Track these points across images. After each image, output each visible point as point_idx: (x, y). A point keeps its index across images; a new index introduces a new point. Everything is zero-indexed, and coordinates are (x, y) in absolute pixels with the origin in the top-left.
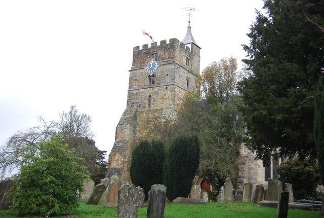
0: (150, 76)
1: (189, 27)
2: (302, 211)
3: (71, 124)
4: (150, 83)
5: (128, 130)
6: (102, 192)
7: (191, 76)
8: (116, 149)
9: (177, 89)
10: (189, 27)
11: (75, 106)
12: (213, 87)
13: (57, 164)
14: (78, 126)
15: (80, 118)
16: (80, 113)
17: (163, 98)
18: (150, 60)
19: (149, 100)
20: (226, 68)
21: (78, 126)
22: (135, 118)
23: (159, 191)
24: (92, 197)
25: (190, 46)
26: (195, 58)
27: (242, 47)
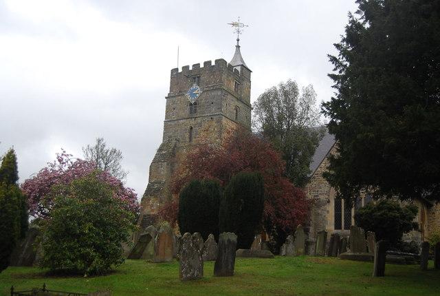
0: (191, 104)
1: (238, 47)
2: (356, 263)
3: (97, 160)
4: (191, 113)
5: (164, 170)
6: (147, 243)
7: (240, 105)
8: (150, 191)
9: (224, 121)
10: (238, 47)
11: (102, 139)
12: (272, 116)
13: (97, 207)
14: (106, 164)
15: (109, 154)
16: (109, 147)
17: (207, 131)
18: (192, 85)
19: (190, 133)
20: (286, 94)
21: (106, 164)
22: (173, 154)
23: (229, 240)
24: (134, 250)
25: (239, 69)
26: (245, 83)
27: (329, 59)
